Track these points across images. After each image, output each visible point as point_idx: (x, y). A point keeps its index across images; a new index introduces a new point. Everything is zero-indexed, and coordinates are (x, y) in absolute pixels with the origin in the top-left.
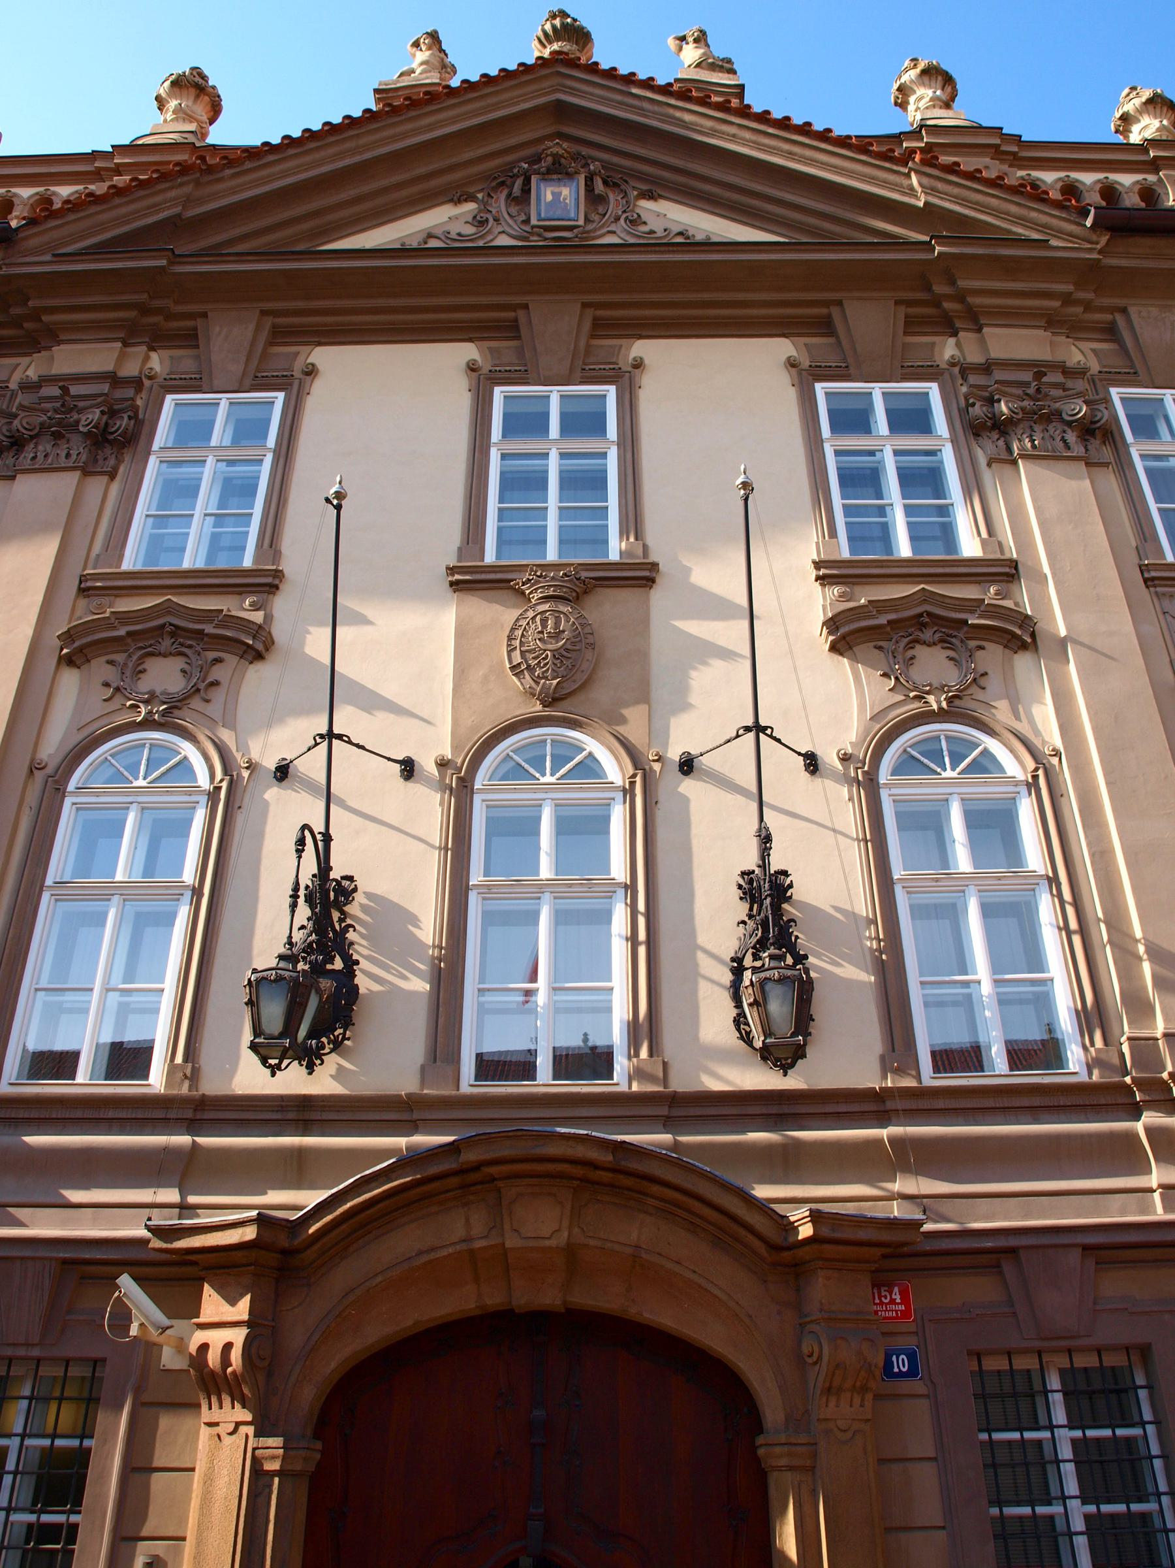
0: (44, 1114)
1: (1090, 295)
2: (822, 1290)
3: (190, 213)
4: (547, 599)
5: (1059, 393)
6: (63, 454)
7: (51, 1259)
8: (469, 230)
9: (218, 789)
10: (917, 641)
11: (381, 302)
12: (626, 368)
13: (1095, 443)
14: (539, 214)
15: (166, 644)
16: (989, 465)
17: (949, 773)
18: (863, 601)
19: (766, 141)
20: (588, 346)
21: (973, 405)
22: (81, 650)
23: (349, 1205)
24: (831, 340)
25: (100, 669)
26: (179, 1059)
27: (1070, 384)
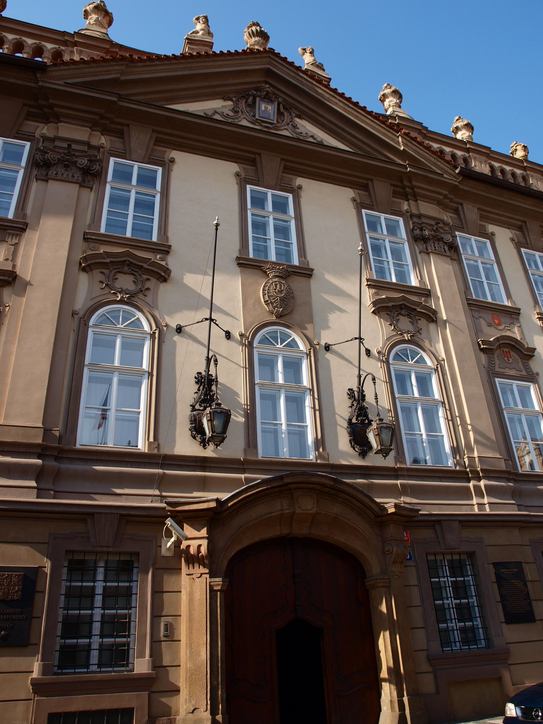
0: (99, 458)
1: (453, 197)
2: (392, 530)
3: (123, 78)
4: (276, 276)
5: (441, 231)
6: (70, 175)
7: (117, 514)
9: (154, 333)
10: (400, 314)
11: (203, 138)
13: (452, 251)
14: (259, 114)
15: (126, 268)
16: (420, 253)
17: (279, 346)
18: (384, 296)
19: (348, 109)
21: (416, 230)
22: (89, 265)
23: (243, 496)
25: (97, 275)
26: (151, 439)
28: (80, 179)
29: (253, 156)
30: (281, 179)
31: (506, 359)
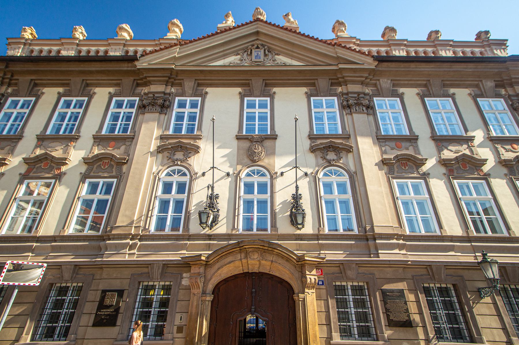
8: (239, 62)
25: (166, 154)
27: (365, 97)
28: (159, 110)
29: (314, 81)
30: (264, 90)
31: (403, 167)
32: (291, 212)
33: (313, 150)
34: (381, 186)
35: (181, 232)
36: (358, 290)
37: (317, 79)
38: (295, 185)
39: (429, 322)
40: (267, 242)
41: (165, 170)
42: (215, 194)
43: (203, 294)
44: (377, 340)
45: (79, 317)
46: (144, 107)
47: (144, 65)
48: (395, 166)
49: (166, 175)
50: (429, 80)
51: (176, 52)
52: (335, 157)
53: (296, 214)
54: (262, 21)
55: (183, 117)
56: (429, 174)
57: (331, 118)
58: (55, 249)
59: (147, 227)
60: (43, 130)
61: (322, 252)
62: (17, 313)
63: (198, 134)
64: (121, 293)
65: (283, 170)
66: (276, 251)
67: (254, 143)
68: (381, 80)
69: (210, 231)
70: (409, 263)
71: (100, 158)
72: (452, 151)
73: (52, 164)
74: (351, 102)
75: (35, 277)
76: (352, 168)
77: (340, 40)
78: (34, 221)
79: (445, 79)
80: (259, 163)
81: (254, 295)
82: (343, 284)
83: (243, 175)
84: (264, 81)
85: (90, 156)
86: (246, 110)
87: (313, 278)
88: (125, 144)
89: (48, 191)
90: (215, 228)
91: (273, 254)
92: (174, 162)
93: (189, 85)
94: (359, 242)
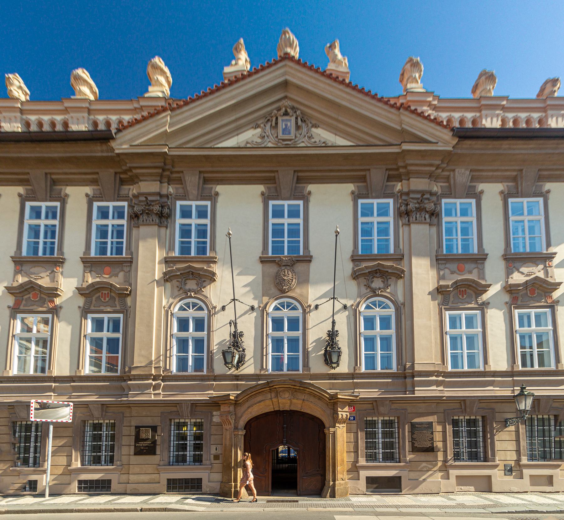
6: (151, 220)
8: (259, 140)
12: (306, 195)
16: (402, 226)
20: (296, 186)
24: (365, 184)
28: (157, 221)
29: (272, 175)
30: (295, 189)
31: (460, 296)
32: (326, 351)
33: (355, 276)
34: (430, 320)
35: (205, 373)
36: (388, 424)
37: (369, 170)
38: (331, 320)
39: (450, 447)
40: (298, 381)
41: (177, 303)
42: (239, 331)
43: (234, 429)
44: (399, 462)
45: (120, 448)
46: (408, 213)
47: (124, 147)
48: (451, 295)
49: (180, 309)
50: (521, 170)
51: (166, 123)
52: (382, 285)
53: (331, 353)
54: (292, 59)
55: (190, 231)
56: (488, 303)
57: (383, 231)
58: (75, 389)
59: (168, 368)
60: (17, 249)
61: (355, 390)
62: (60, 444)
63: (211, 255)
64: (154, 429)
65: (318, 302)
66: (307, 390)
67: (283, 268)
68: (457, 170)
69: (236, 371)
70: (444, 398)
71: (97, 289)
72: (523, 273)
73: (42, 295)
74: (411, 206)
75: (65, 414)
76: (401, 298)
77: (409, 98)
78: (44, 362)
79: (544, 167)
80: (289, 294)
81: (285, 430)
82: (374, 419)
83: (270, 309)
84: (296, 174)
85: (84, 286)
86: (272, 221)
87: (344, 414)
88: (123, 270)
89: (48, 328)
90: (241, 368)
91: (305, 393)
92: (186, 293)
93: (192, 180)
94: (396, 380)
